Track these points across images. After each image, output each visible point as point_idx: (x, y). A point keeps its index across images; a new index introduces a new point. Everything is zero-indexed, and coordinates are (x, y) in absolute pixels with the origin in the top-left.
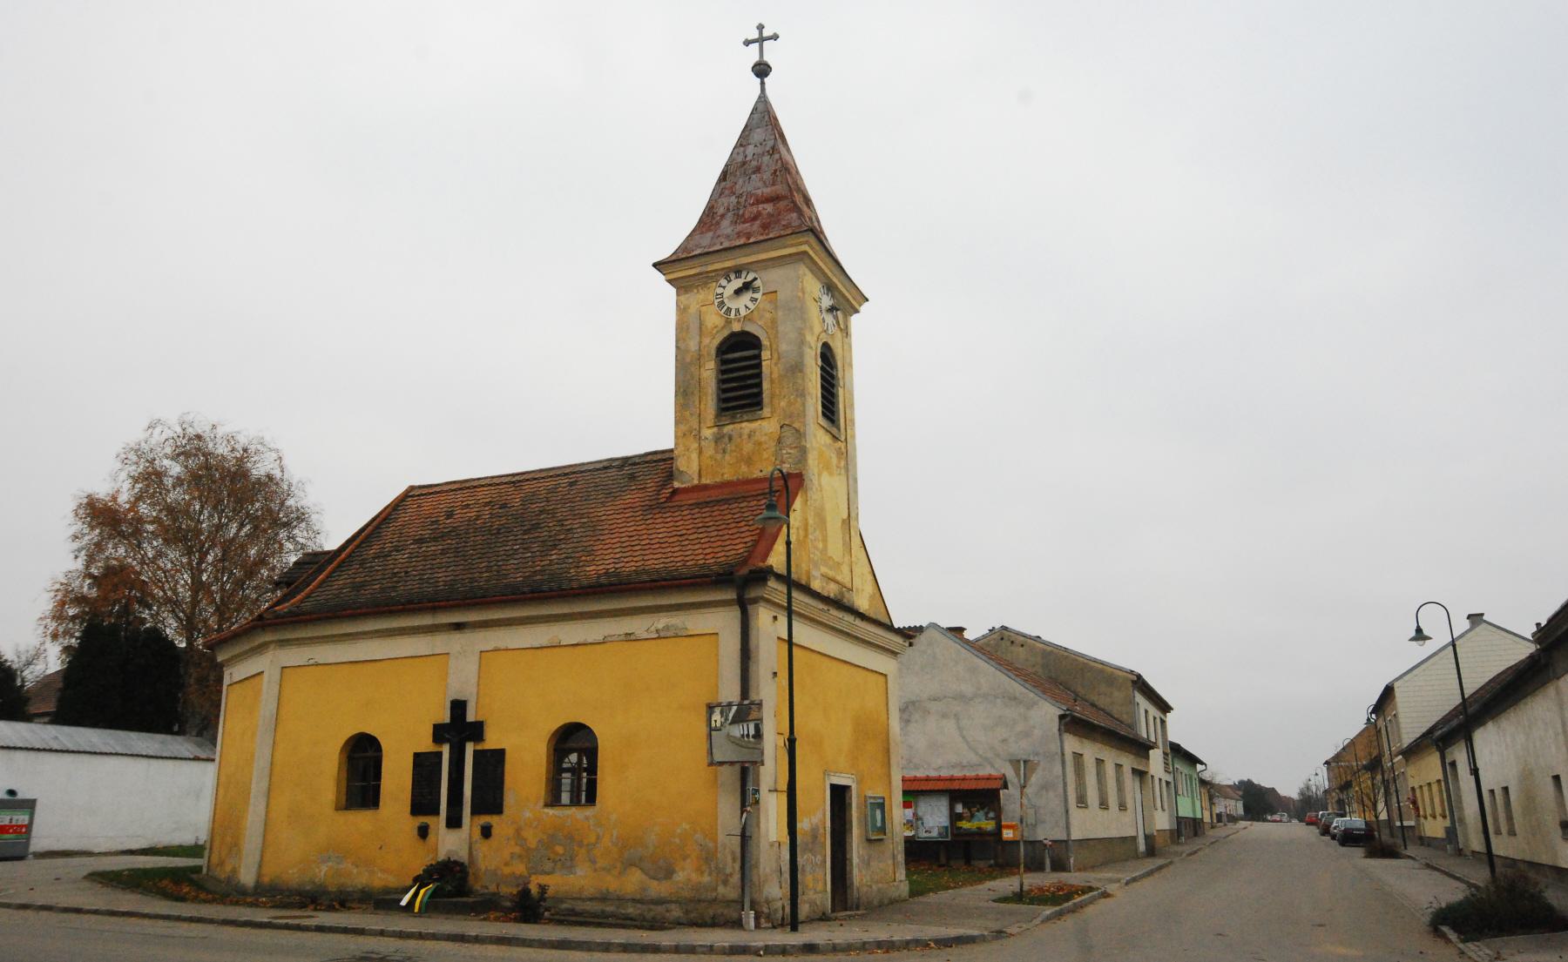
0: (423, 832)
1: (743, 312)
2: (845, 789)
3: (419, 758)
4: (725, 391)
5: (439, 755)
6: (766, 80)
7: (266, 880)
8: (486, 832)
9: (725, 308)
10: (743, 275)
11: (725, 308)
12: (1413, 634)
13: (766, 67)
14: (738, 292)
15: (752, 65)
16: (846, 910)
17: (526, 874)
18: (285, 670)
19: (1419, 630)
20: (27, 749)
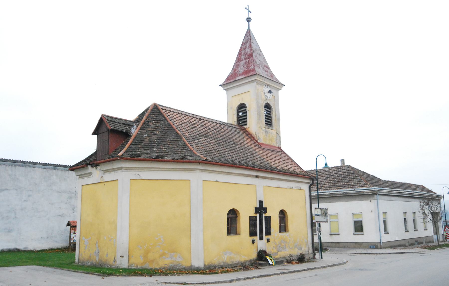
0: (253, 242)
2: (281, 231)
3: (251, 218)
5: (256, 217)
6: (250, 23)
7: (207, 264)
8: (268, 241)
17: (277, 252)
18: (84, 187)
20: (378, 205)
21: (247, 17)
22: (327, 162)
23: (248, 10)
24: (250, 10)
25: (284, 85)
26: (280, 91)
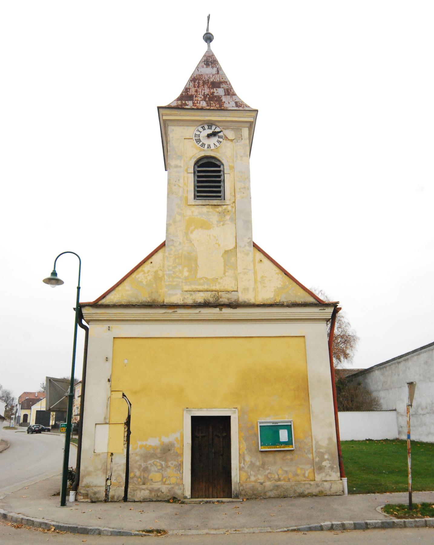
1: (213, 147)
4: (198, 187)
9: (201, 143)
10: (213, 127)
11: (201, 143)
13: (210, 35)
14: (209, 136)
16: (231, 497)
19: (54, 273)
22: (56, 269)
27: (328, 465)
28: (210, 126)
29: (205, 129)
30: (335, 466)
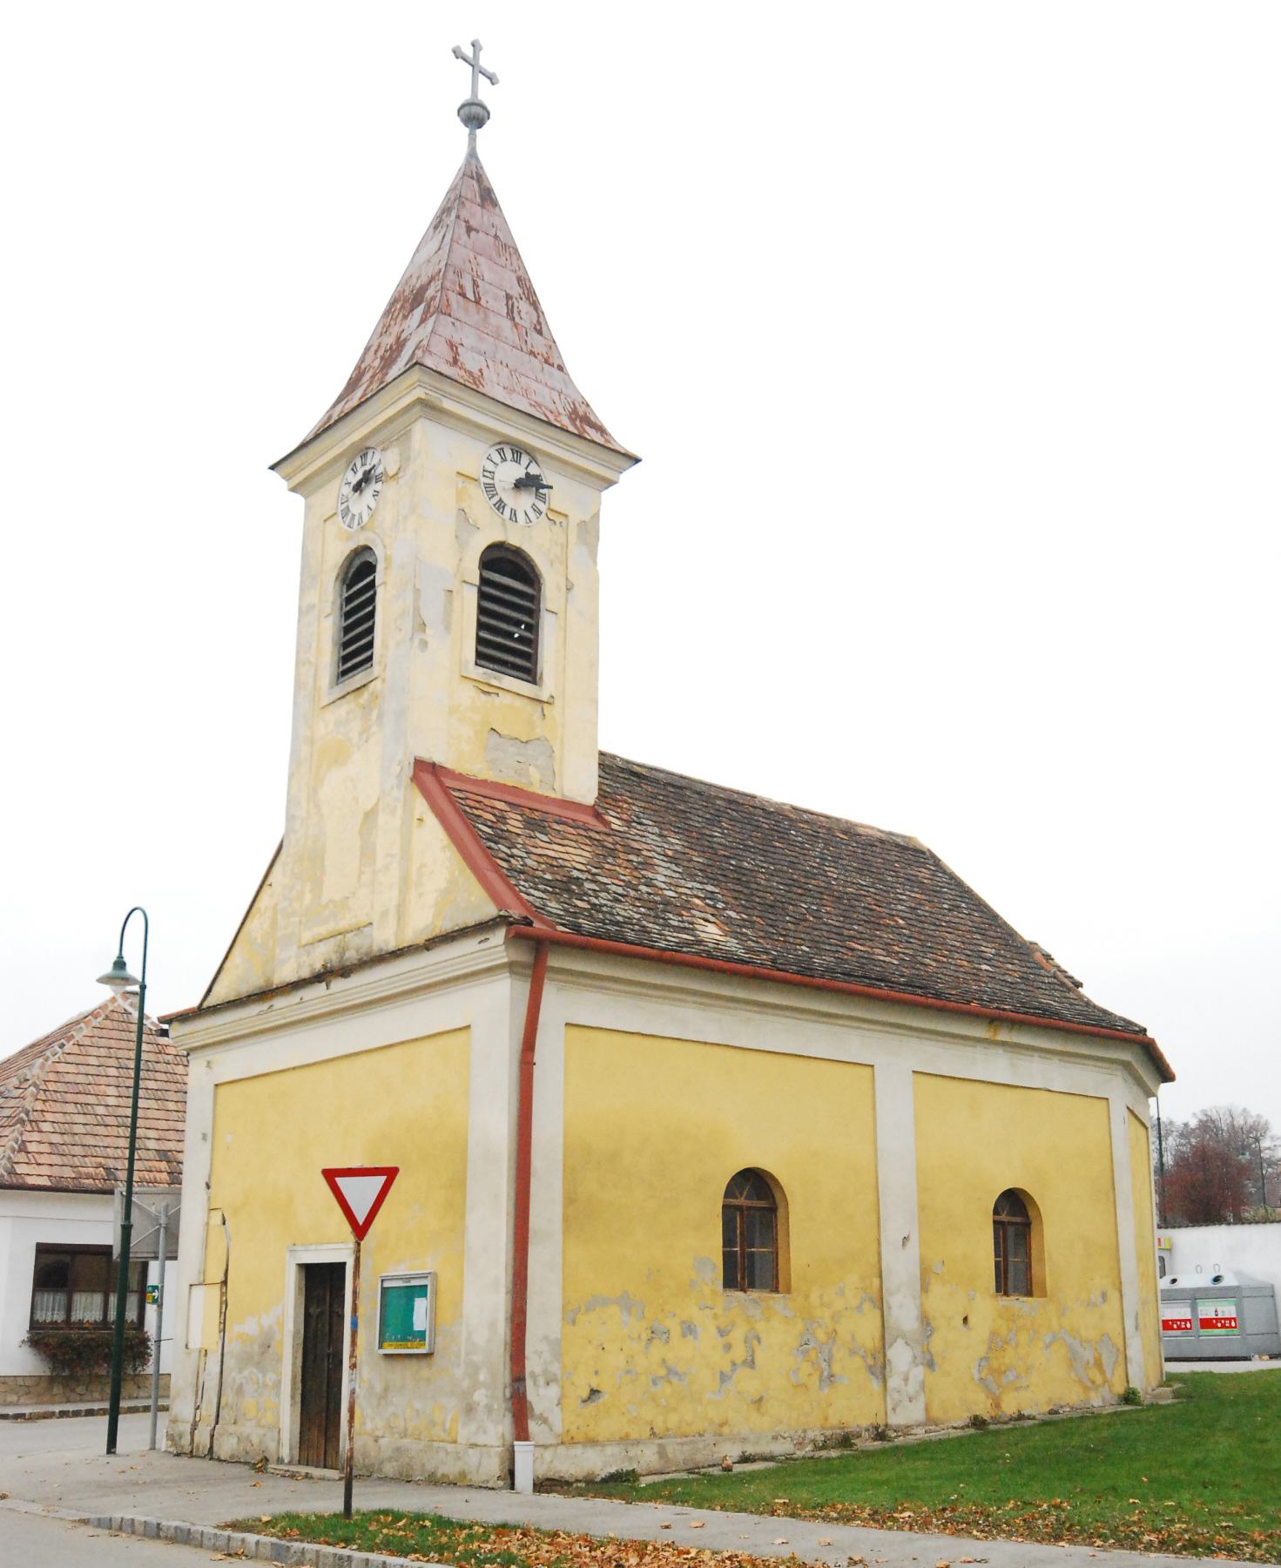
12: (108, 969)
13: (486, 114)
15: (458, 105)
18: (222, 1090)
21: (466, 96)
22: (124, 954)
23: (473, 64)
24: (485, 62)
25: (637, 460)
26: (608, 495)
27: (484, 1401)
28: (517, 452)
29: (506, 460)
30: (496, 1407)
